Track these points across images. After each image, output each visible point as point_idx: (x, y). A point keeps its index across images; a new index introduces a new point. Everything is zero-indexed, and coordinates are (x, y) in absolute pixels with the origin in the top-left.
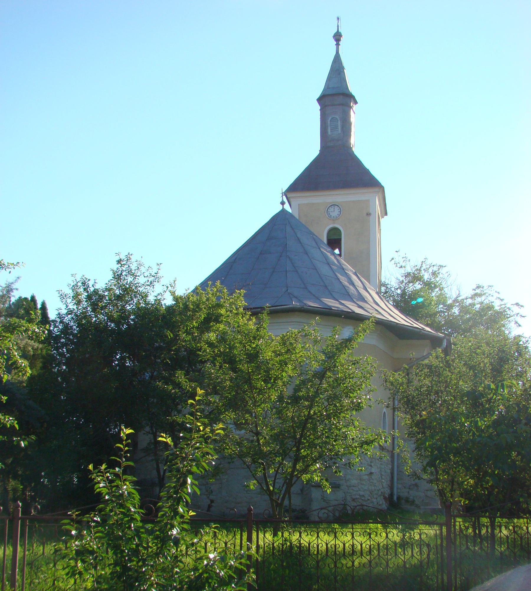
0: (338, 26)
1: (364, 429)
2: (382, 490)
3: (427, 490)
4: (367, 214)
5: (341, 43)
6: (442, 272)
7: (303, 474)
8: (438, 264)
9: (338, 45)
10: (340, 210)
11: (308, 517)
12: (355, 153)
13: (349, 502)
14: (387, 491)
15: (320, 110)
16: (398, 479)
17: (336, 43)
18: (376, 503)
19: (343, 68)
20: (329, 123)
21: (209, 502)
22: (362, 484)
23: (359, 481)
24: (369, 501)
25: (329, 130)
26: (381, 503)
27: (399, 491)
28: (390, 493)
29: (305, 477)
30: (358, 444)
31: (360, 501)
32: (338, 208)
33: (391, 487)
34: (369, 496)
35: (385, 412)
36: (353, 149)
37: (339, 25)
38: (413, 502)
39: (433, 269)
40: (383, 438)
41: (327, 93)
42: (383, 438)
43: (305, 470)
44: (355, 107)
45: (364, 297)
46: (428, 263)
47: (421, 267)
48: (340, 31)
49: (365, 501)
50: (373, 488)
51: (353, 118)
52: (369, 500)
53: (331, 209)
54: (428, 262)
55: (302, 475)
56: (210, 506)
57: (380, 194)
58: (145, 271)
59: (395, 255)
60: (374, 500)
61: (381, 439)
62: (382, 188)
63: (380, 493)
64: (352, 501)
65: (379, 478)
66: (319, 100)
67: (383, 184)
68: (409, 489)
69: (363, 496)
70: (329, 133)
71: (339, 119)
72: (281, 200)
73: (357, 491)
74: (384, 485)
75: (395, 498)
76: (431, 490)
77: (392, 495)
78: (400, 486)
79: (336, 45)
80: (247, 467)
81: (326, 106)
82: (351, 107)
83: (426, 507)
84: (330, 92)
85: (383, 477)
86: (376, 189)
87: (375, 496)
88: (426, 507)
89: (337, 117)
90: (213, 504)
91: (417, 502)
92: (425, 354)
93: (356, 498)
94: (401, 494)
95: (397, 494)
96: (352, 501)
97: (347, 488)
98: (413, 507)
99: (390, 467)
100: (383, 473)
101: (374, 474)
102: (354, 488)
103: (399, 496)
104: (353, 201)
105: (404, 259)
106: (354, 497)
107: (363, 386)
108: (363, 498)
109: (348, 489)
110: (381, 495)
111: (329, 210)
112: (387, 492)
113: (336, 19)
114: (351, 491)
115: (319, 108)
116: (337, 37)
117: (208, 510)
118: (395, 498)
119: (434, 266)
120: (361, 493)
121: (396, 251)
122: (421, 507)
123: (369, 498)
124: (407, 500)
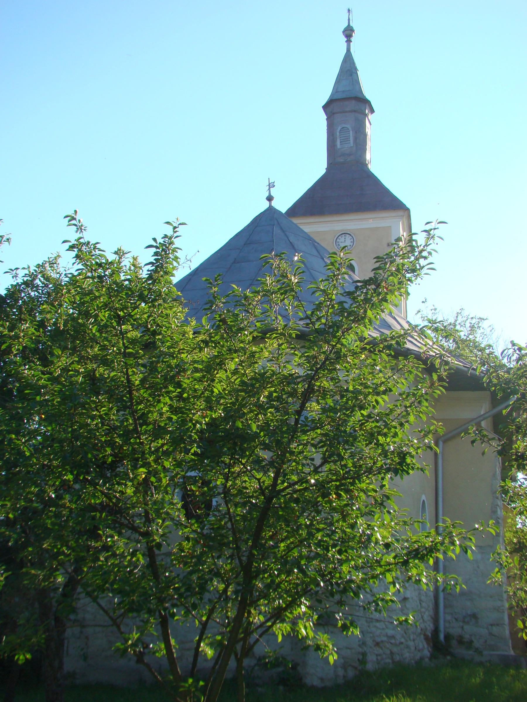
0: (349, 20)
1: (405, 523)
3: (492, 625)
4: (388, 245)
5: (352, 39)
6: (483, 326)
8: (478, 316)
9: (349, 41)
10: (352, 240)
11: (301, 679)
12: (371, 170)
13: (371, 647)
14: (429, 626)
15: (327, 119)
16: (445, 607)
17: (346, 40)
18: (413, 649)
19: (356, 69)
20: (338, 134)
24: (402, 646)
25: (338, 143)
26: (421, 646)
27: (447, 625)
28: (433, 629)
30: (394, 558)
31: (388, 645)
32: (350, 237)
33: (436, 619)
34: (403, 636)
35: (424, 501)
37: (351, 19)
39: (471, 322)
40: (458, 542)
42: (458, 542)
44: (370, 117)
45: (390, 324)
46: (465, 315)
47: (456, 321)
49: (395, 645)
51: (369, 130)
52: (402, 643)
53: (342, 239)
54: (465, 313)
55: (274, 623)
57: (404, 219)
59: (422, 307)
60: (411, 644)
61: (453, 543)
62: (408, 210)
63: (419, 631)
64: (375, 646)
65: (417, 606)
66: (325, 107)
67: (408, 206)
68: (464, 622)
69: (393, 637)
70: (339, 146)
71: (350, 129)
72: (267, 195)
73: (383, 629)
74: (426, 617)
75: (442, 637)
76: (498, 625)
77: (436, 631)
78: (448, 617)
79: (346, 41)
80: (110, 622)
81: (334, 114)
82: (366, 115)
83: (492, 653)
84: (338, 96)
85: (424, 604)
86: (400, 213)
87: (412, 637)
88: (492, 653)
89: (348, 126)
91: (477, 644)
92: (482, 413)
93: (382, 641)
94: (451, 631)
95: (445, 631)
96: (375, 646)
97: (366, 624)
98: (471, 652)
100: (423, 598)
101: (410, 600)
102: (378, 624)
103: (448, 633)
104: (371, 228)
105: (433, 311)
106: (378, 640)
107: (412, 418)
108: (393, 641)
109: (369, 626)
110: (420, 634)
111: (338, 240)
112: (430, 626)
113: (347, 11)
114: (374, 629)
115: (326, 117)
116: (348, 32)
118: (442, 637)
119: (472, 318)
120: (390, 632)
121: (423, 302)
123: (403, 640)
124: (461, 641)
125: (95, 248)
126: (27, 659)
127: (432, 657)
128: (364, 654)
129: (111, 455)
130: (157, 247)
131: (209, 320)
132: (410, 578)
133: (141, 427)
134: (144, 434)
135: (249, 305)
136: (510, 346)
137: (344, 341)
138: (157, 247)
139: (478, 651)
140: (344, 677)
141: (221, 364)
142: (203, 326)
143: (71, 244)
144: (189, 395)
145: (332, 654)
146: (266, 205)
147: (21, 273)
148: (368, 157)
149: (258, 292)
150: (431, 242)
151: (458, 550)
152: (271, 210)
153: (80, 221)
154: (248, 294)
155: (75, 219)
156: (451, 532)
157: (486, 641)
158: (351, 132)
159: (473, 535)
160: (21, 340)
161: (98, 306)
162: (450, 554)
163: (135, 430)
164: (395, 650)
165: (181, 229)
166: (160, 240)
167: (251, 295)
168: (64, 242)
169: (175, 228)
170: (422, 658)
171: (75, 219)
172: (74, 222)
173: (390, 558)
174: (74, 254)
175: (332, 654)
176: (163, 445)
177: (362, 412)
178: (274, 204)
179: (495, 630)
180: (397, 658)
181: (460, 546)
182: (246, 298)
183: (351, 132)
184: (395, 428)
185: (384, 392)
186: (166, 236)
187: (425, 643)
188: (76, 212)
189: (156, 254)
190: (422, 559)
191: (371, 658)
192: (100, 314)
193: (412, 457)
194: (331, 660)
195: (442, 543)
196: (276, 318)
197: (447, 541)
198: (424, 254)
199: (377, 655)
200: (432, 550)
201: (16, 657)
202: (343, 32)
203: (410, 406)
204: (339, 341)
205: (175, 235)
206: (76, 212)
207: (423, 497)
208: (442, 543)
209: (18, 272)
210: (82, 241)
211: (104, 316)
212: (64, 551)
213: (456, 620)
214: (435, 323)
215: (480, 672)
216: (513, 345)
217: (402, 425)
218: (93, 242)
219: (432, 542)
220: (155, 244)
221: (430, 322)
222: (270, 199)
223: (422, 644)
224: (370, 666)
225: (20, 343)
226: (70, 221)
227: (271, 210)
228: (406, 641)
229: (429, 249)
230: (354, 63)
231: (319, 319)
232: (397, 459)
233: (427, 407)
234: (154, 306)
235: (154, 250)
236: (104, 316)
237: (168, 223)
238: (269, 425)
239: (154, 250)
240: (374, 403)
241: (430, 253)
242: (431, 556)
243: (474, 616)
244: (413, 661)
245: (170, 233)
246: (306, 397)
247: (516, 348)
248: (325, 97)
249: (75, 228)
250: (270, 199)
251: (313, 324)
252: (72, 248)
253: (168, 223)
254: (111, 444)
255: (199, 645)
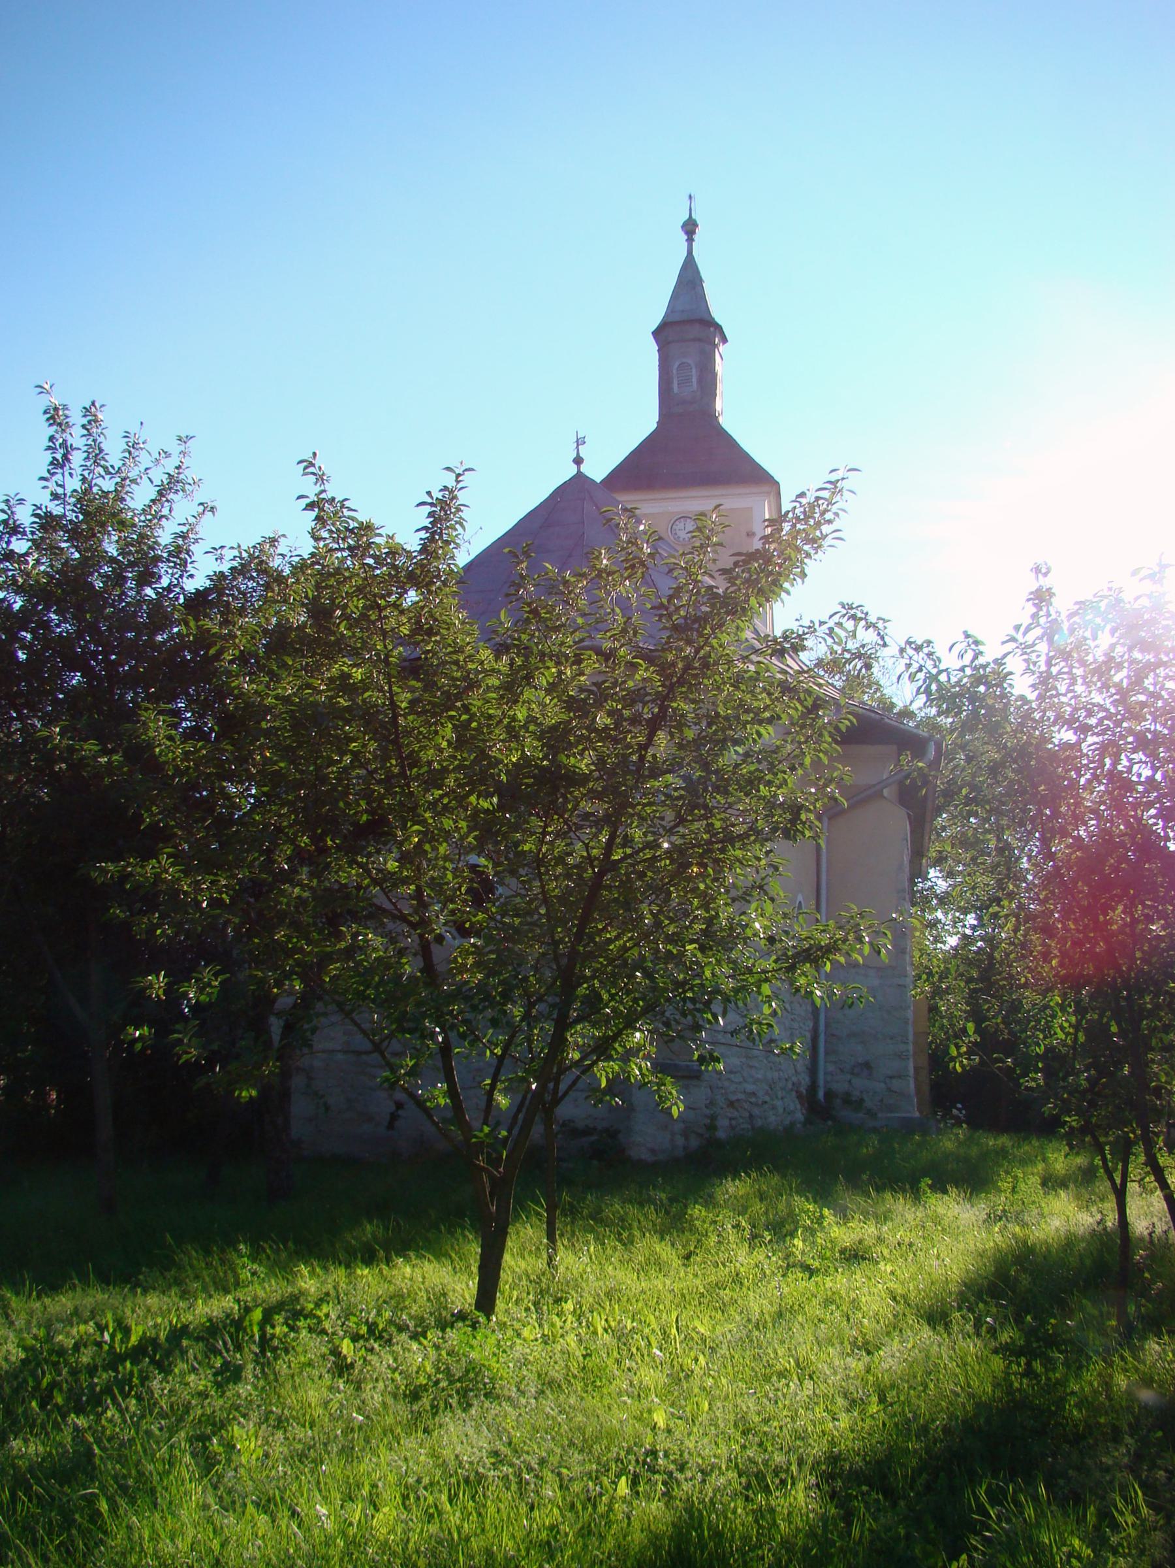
2: (794, 1079)
3: (891, 1077)
5: (696, 237)
7: (598, 1059)
9: (690, 240)
16: (827, 1053)
18: (781, 1110)
19: (701, 280)
21: (393, 1108)
22: (751, 1067)
23: (744, 1060)
24: (766, 1106)
27: (829, 1078)
29: (604, 1072)
30: (776, 961)
31: (746, 1106)
33: (813, 1070)
34: (767, 1093)
36: (721, 420)
38: (858, 1104)
40: (867, 939)
41: (670, 320)
42: (867, 939)
43: (601, 1049)
44: (722, 348)
48: (694, 216)
49: (757, 1105)
50: (776, 1075)
53: (680, 525)
55: (595, 1063)
56: (394, 1117)
58: (151, 465)
60: (779, 1103)
61: (860, 939)
62: (777, 484)
63: (790, 1085)
66: (656, 334)
67: (776, 478)
68: (852, 1074)
69: (754, 1094)
73: (740, 1083)
75: (821, 1095)
76: (900, 1077)
77: (813, 1087)
78: (831, 1068)
82: (716, 346)
86: (765, 488)
87: (780, 1094)
89: (690, 361)
90: (400, 1112)
91: (868, 1104)
93: (738, 1100)
98: (861, 1115)
99: (811, 1024)
106: (733, 1098)
108: (753, 1100)
112: (805, 1080)
116: (690, 228)
117: (391, 1126)
118: (821, 1095)
120: (750, 1088)
122: (880, 1115)
123: (767, 1098)
124: (847, 1100)
125: (343, 506)
126: (251, 1097)
127: (808, 1122)
128: (713, 1118)
129: (366, 811)
130: (432, 505)
131: (510, 613)
132: (798, 990)
133: (410, 770)
134: (414, 780)
135: (570, 593)
136: (962, 638)
137: (714, 642)
138: (432, 505)
139: (871, 1114)
140: (685, 1148)
141: (528, 678)
142: (501, 623)
143: (308, 501)
144: (479, 724)
145: (676, 1104)
146: (572, 470)
147: (229, 554)
148: (718, 406)
149: (583, 575)
150: (838, 498)
151: (867, 949)
152: (580, 478)
153: (320, 468)
154: (567, 577)
155: (313, 465)
156: (859, 925)
157: (882, 1101)
158: (694, 370)
159: (888, 928)
160: (237, 641)
161: (347, 593)
162: (855, 956)
163: (403, 774)
164: (756, 1111)
165: (467, 478)
166: (437, 495)
167: (573, 579)
168: (300, 497)
169: (458, 475)
170: (792, 1124)
171: (313, 465)
172: (311, 470)
173: (769, 964)
174: (313, 514)
175: (676, 1104)
176: (442, 797)
177: (737, 748)
178: (584, 468)
179: (896, 1084)
180: (759, 1123)
181: (870, 943)
182: (566, 583)
183: (694, 370)
184: (785, 772)
185: (770, 721)
186: (445, 488)
187: (797, 1102)
188: (315, 454)
189: (431, 514)
190: (816, 962)
191: (723, 1123)
192: (350, 604)
193: (809, 810)
194: (675, 1112)
195: (845, 940)
196: (613, 610)
197: (851, 937)
198: (828, 516)
199: (731, 1119)
200: (832, 948)
201: (236, 1093)
202: (682, 227)
203: (806, 742)
204: (706, 643)
205: (460, 486)
206: (315, 454)
207: (800, 898)
208: (845, 940)
209: (224, 551)
210: (323, 496)
211: (357, 607)
212: (302, 948)
213: (842, 1070)
214: (852, 608)
215: (875, 1140)
216: (967, 636)
217: (793, 769)
218: (339, 498)
219: (831, 938)
220: (430, 501)
221: (844, 607)
222: (578, 461)
223: (794, 1104)
224: (721, 1134)
225: (236, 646)
226: (305, 468)
227: (580, 478)
228: (772, 1099)
229: (834, 508)
230: (698, 272)
231: (678, 609)
232: (788, 816)
233: (830, 744)
234: (430, 592)
235: (428, 509)
236: (357, 607)
237: (448, 469)
238: (605, 763)
239: (428, 509)
240: (755, 736)
241: (836, 514)
242: (828, 959)
243: (867, 1065)
244: (780, 1128)
245: (451, 483)
246: (654, 725)
247: (971, 640)
248: (656, 318)
249: (313, 478)
250: (578, 461)
251: (670, 616)
252: (310, 506)
253: (448, 469)
254: (368, 795)
255: (490, 1094)
